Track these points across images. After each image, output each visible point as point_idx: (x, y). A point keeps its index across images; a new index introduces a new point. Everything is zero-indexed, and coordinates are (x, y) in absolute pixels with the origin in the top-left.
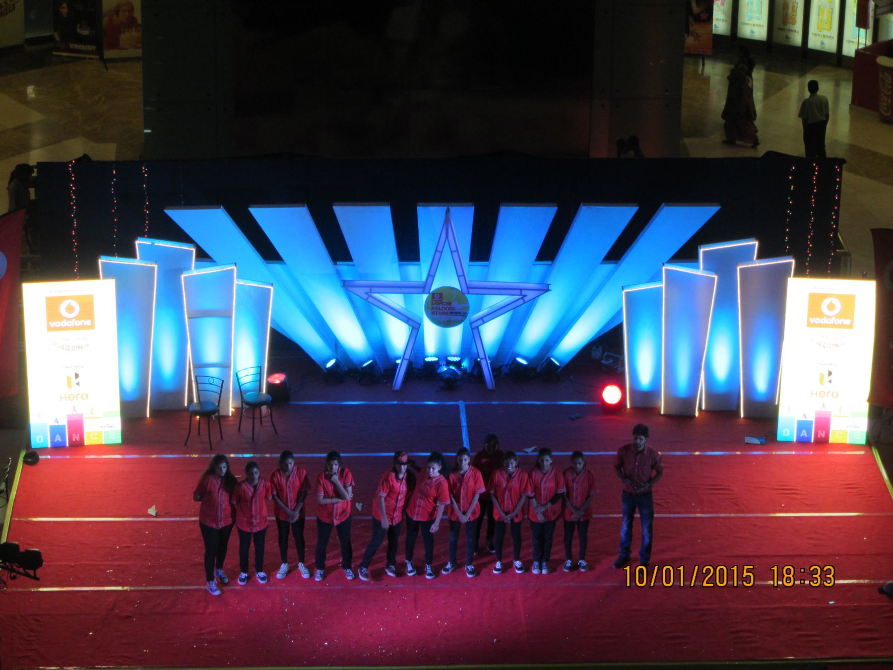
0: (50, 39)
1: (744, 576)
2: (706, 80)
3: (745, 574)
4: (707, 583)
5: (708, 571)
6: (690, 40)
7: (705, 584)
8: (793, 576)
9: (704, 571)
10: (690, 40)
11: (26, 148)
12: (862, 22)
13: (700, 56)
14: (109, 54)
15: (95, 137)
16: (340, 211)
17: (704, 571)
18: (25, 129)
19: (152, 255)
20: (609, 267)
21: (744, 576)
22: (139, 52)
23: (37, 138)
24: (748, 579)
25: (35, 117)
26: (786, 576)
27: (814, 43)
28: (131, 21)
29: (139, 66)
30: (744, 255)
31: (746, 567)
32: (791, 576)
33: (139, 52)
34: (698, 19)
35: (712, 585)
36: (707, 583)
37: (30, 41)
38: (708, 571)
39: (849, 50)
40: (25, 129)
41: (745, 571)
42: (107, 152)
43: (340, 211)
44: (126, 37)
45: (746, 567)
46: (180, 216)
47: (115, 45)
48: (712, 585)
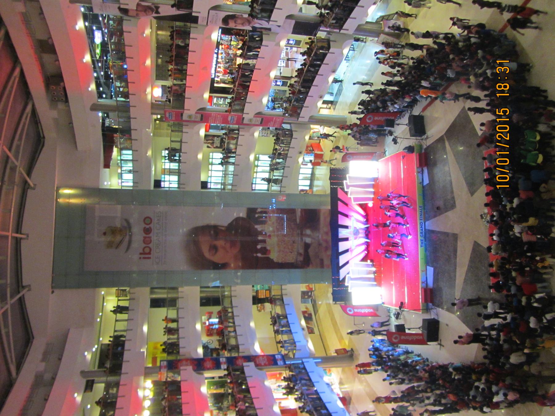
0: (311, 300)
1: (503, 114)
2: (317, 190)
3: (501, 113)
4: (507, 137)
5: (500, 136)
6: (310, 193)
7: (508, 139)
8: (503, 84)
9: (500, 139)
10: (310, 193)
11: (330, 304)
12: (306, 165)
13: (312, 192)
14: (314, 290)
15: (328, 291)
16: (340, 251)
17: (500, 139)
18: (327, 304)
19: (348, 283)
20: (349, 206)
21: (503, 114)
22: (313, 285)
23: (328, 302)
24: (505, 112)
25: (324, 302)
26: (503, 88)
27: (310, 173)
28: (308, 286)
29: (316, 285)
30: (346, 183)
31: (497, 113)
32: (503, 85)
33: (313, 285)
34: (307, 192)
35: (508, 134)
36: (507, 137)
37: (312, 303)
38: (500, 136)
39: (311, 167)
40: (327, 304)
41: (500, 114)
42: (331, 290)
43: (340, 251)
44: (311, 287)
45: (497, 113)
46: (341, 278)
47: (312, 289)
48: (508, 134)
